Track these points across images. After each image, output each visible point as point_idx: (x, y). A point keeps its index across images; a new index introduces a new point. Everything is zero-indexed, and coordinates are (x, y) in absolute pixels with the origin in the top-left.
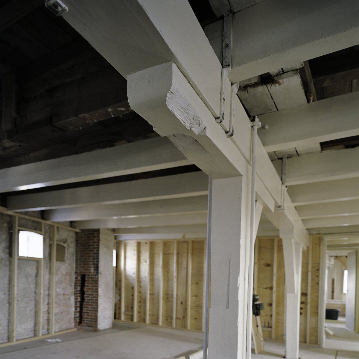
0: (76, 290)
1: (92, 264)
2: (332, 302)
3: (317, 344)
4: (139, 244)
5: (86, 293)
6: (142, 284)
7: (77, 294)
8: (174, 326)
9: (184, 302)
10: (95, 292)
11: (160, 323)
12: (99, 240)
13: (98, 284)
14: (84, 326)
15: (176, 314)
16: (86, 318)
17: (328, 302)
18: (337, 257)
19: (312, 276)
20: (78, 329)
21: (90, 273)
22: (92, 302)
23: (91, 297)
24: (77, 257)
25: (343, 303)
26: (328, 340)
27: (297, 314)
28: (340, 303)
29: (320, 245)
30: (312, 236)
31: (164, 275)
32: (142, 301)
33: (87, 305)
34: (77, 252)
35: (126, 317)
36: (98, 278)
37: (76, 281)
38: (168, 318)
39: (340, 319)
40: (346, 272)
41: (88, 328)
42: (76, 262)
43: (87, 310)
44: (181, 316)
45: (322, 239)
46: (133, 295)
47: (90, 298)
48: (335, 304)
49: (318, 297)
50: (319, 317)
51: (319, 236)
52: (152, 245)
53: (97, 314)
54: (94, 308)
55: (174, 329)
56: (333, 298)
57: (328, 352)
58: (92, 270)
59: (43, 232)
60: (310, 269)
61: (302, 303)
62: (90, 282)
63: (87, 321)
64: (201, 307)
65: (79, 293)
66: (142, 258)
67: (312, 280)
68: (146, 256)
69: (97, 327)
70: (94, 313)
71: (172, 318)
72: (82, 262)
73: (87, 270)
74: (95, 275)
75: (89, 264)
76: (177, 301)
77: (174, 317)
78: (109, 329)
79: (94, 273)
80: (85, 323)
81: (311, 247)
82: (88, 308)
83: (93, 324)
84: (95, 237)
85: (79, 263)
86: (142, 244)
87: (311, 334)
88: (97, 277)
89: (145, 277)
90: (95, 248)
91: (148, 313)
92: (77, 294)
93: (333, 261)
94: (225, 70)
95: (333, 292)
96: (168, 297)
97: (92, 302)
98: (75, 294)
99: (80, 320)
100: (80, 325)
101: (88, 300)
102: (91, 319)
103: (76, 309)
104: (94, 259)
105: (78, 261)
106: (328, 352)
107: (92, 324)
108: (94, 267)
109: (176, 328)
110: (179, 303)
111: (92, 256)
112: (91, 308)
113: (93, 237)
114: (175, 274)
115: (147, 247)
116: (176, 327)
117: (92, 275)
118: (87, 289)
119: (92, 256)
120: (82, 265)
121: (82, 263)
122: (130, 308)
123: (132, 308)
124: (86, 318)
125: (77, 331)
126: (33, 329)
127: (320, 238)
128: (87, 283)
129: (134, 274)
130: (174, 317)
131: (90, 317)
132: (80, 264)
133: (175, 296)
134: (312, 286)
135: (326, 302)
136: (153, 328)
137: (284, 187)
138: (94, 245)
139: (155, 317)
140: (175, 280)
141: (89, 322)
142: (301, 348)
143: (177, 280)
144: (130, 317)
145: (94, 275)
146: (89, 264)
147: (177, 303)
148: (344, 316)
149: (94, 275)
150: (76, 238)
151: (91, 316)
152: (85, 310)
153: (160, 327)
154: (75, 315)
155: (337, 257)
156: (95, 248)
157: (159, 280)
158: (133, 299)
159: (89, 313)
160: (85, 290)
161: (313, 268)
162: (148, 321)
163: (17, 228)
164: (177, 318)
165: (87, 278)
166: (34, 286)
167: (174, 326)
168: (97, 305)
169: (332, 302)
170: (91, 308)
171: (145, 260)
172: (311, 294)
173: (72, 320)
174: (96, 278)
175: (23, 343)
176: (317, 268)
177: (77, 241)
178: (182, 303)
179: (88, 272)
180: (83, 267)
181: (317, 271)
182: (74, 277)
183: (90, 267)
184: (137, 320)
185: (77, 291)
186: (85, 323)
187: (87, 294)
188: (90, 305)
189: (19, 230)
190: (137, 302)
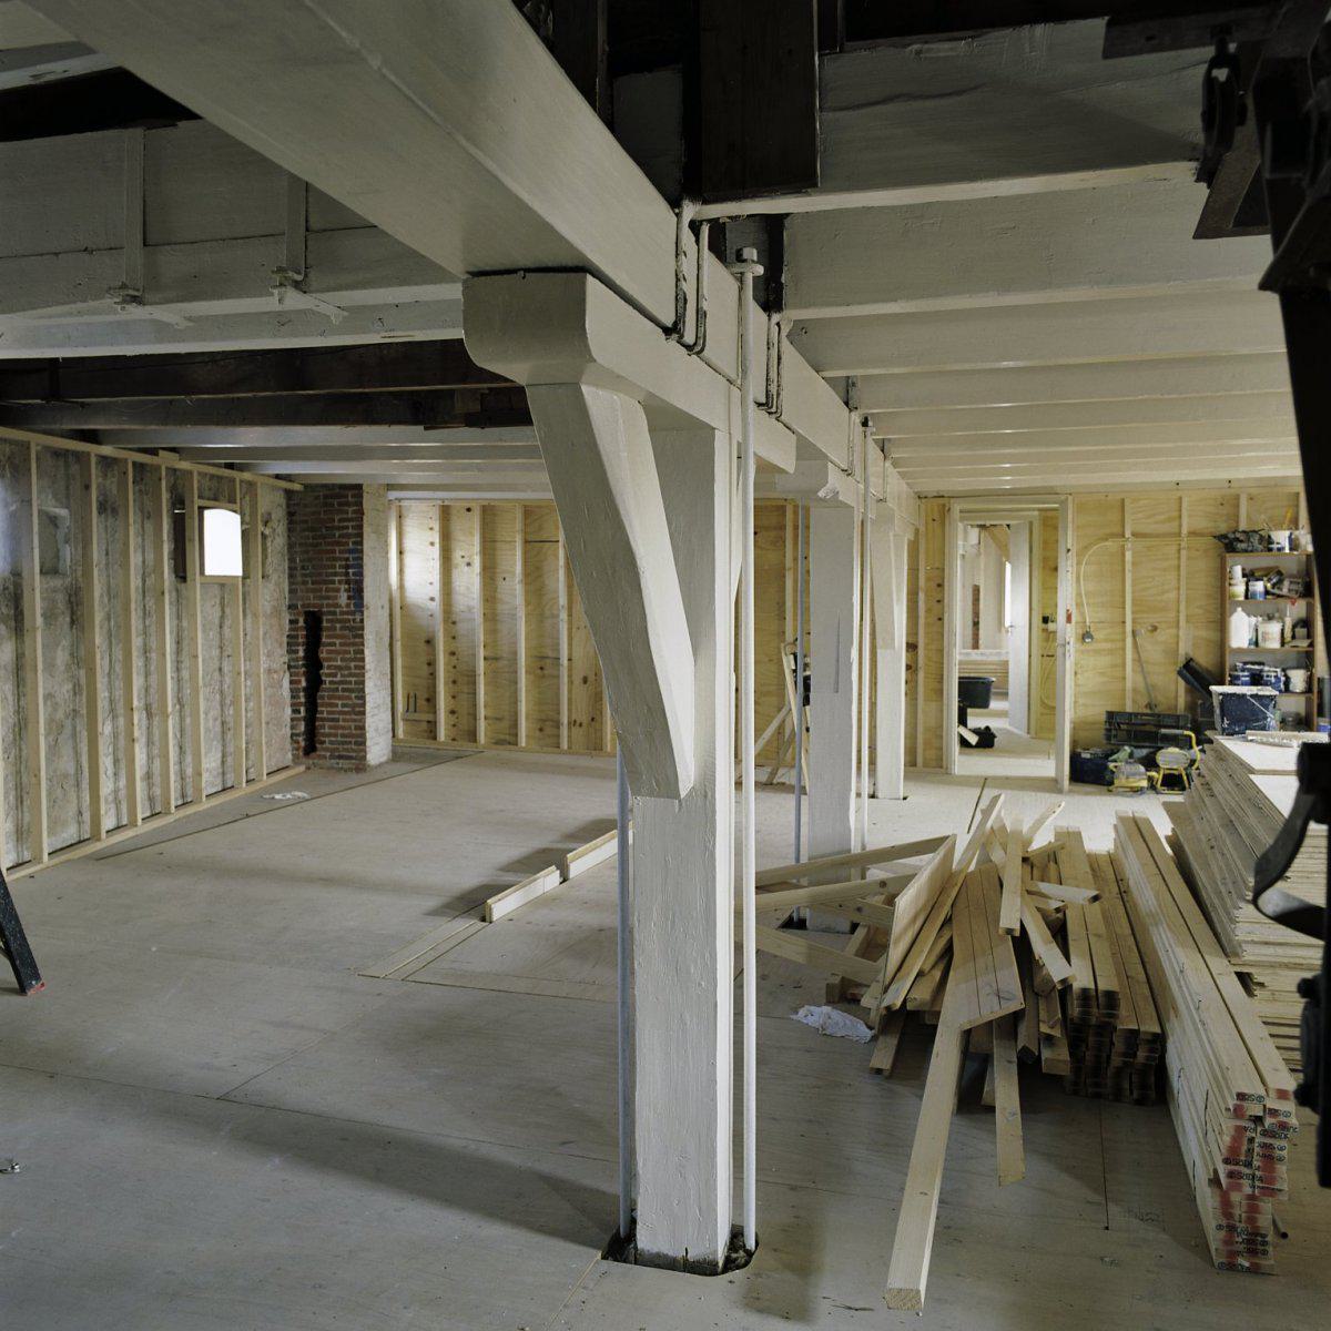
0: (294, 656)
1: (340, 582)
2: (975, 655)
3: (941, 767)
4: (446, 513)
5: (326, 664)
6: (462, 628)
7: (295, 667)
8: (565, 745)
9: (591, 678)
10: (355, 660)
11: (523, 742)
12: (361, 512)
13: (362, 636)
14: (320, 757)
15: (570, 710)
16: (329, 735)
17: (963, 658)
18: (982, 527)
19: (926, 602)
20: (308, 768)
21: (337, 605)
22: (344, 690)
23: (342, 676)
24: (292, 560)
25: (1003, 658)
26: (964, 758)
27: (900, 695)
28: (996, 659)
29: (943, 524)
30: (923, 501)
31: (528, 603)
32: (464, 680)
33: (330, 697)
34: (291, 546)
35: (444, 727)
36: (362, 621)
37: (290, 630)
38: (547, 725)
39: (995, 704)
40: (1008, 566)
41: (338, 764)
42: (291, 576)
43: (328, 713)
44: (584, 718)
45: (949, 510)
46: (431, 664)
47: (339, 678)
48: (979, 660)
49: (941, 651)
50: (945, 701)
51: (941, 501)
52: (489, 515)
53: (363, 721)
54: (354, 706)
55: (565, 753)
56: (976, 646)
57: (966, 781)
58: (343, 599)
59: (237, 507)
60: (922, 582)
61: (908, 667)
62: (338, 632)
63: (331, 743)
64: (43, 645)
65: (303, 665)
66: (457, 555)
67: (928, 611)
68: (469, 548)
69: (364, 758)
70: (355, 721)
71: (557, 725)
72: (310, 575)
73: (328, 598)
74: (353, 613)
75: (333, 582)
76: (570, 676)
77: (565, 720)
78: (387, 762)
79: (348, 605)
80: (327, 749)
81: (922, 529)
82: (337, 705)
83: (354, 751)
84: (348, 504)
85: (299, 579)
86: (454, 512)
87: (927, 743)
88: (358, 617)
89: (470, 609)
90: (349, 536)
91: (482, 712)
92: (295, 667)
93: (974, 534)
94: (853, 414)
95: (976, 624)
96: (544, 665)
97: (344, 690)
98: (289, 667)
99: (309, 743)
100: (313, 755)
101: (331, 682)
102: (343, 736)
103: (296, 711)
104: (347, 567)
105: (298, 573)
106: (966, 781)
107: (347, 750)
108: (348, 590)
109: (570, 751)
110: (578, 680)
111: (340, 559)
112: (344, 705)
113: (340, 504)
114: (563, 600)
115: (475, 520)
116: (569, 748)
117: (342, 613)
118: (329, 652)
119: (340, 559)
120: (310, 586)
121: (309, 579)
122: (422, 702)
123: (431, 700)
124: (329, 735)
125: (305, 772)
126: (220, 770)
127: (944, 505)
128: (328, 637)
129: (432, 599)
130: (565, 720)
131: (340, 732)
132: (304, 583)
133: (565, 662)
134: (927, 625)
135: (960, 659)
136: (504, 753)
137: (888, 464)
138: (347, 527)
139: (506, 724)
140: (564, 615)
141: (341, 747)
142: (907, 777)
143: (570, 615)
144: (424, 726)
145: (347, 613)
146: (333, 582)
147: (571, 682)
148: (1004, 695)
149: (347, 613)
150: (288, 506)
151: (343, 728)
152: (323, 712)
153: (523, 750)
154: (292, 727)
155: (982, 527)
156: (349, 536)
157: (513, 616)
158: (433, 675)
159: (338, 720)
160: (323, 655)
161: (928, 579)
162: (482, 737)
163: (198, 502)
164: (572, 723)
165: (328, 621)
166: (218, 651)
167: (565, 745)
168: (363, 698)
169: (975, 655)
170: (344, 705)
171: (466, 560)
172: (927, 645)
173: (288, 745)
174: (354, 620)
175: (906, 721)
176: (940, 582)
177: (290, 514)
178: (585, 680)
179: (328, 605)
180: (314, 591)
181: (939, 589)
182: (287, 617)
183: (338, 590)
184: (1186, 702)
185: (297, 660)
186: (327, 749)
187: (329, 667)
188: (339, 698)
189: (202, 509)
190: (446, 683)
